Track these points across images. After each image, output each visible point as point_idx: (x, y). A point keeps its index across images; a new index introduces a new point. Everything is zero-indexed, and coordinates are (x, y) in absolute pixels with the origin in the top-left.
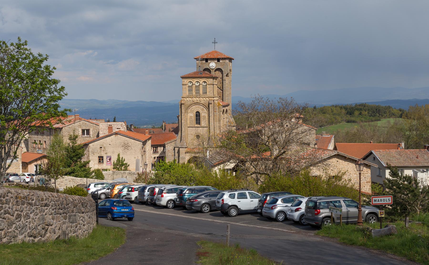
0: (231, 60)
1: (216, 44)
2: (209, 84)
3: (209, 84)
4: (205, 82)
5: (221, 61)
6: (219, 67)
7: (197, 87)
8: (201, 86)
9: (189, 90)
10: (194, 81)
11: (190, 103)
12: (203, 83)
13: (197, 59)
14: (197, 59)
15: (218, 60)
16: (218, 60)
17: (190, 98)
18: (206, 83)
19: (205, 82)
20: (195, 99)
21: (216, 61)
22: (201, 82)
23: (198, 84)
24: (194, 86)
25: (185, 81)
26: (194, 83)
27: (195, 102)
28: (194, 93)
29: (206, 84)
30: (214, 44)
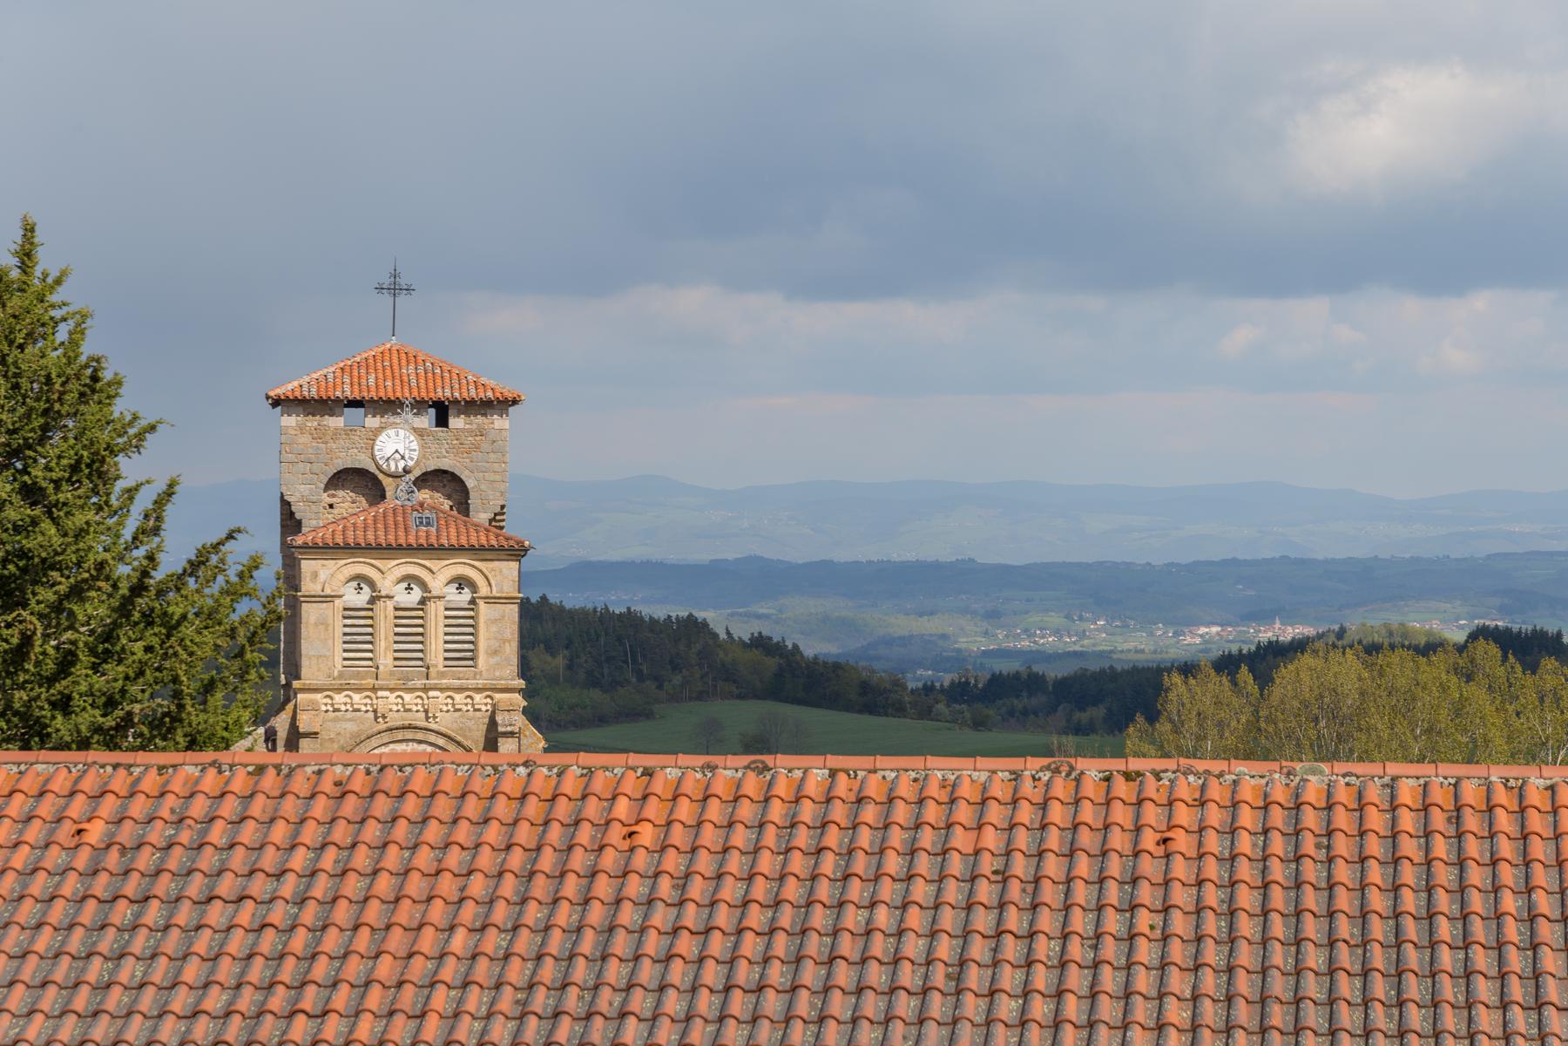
0: (503, 404)
1: (402, 299)
2: (491, 600)
3: (491, 600)
4: (360, 579)
5: (456, 422)
6: (445, 464)
7: (411, 622)
8: (436, 610)
9: (349, 639)
10: (389, 573)
11: (351, 727)
12: (452, 588)
13: (152, 428)
14: (152, 428)
15: (442, 413)
16: (442, 413)
17: (358, 690)
18: (473, 586)
19: (461, 582)
20: (388, 700)
21: (426, 420)
22: (437, 584)
23: (417, 594)
24: (385, 611)
25: (323, 575)
26: (386, 585)
27: (395, 719)
28: (386, 661)
29: (467, 595)
30: (387, 298)
